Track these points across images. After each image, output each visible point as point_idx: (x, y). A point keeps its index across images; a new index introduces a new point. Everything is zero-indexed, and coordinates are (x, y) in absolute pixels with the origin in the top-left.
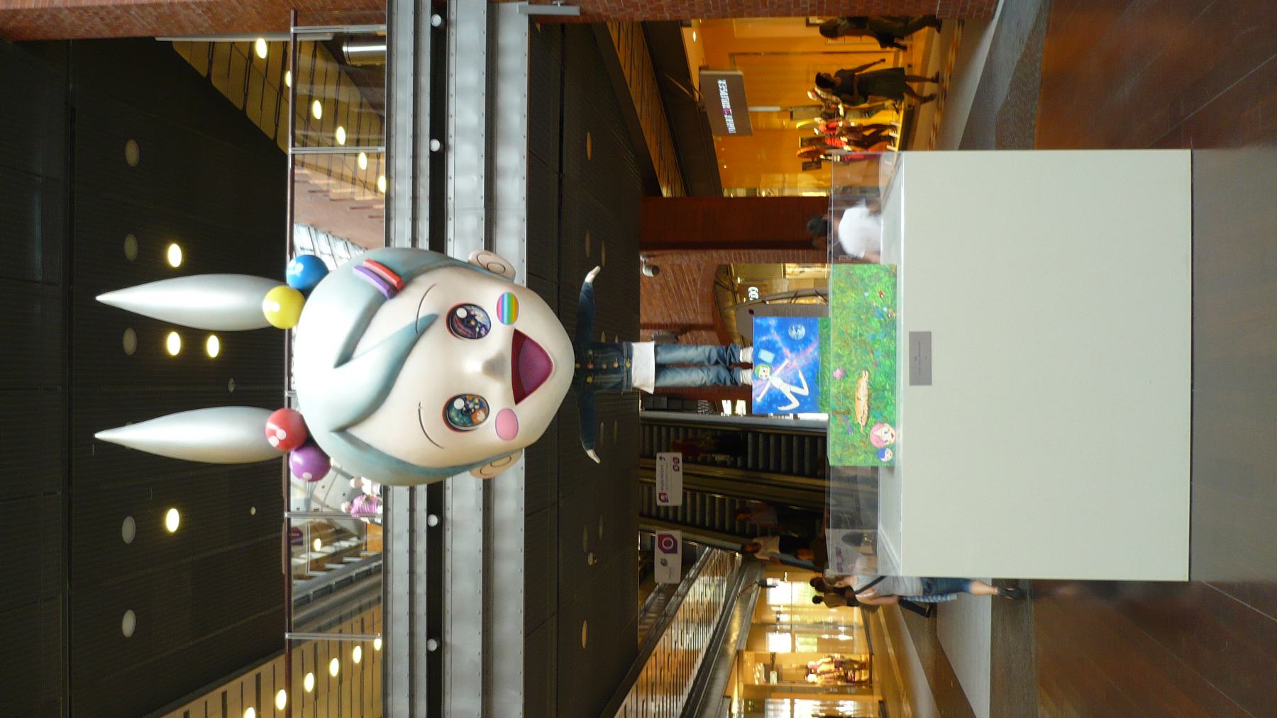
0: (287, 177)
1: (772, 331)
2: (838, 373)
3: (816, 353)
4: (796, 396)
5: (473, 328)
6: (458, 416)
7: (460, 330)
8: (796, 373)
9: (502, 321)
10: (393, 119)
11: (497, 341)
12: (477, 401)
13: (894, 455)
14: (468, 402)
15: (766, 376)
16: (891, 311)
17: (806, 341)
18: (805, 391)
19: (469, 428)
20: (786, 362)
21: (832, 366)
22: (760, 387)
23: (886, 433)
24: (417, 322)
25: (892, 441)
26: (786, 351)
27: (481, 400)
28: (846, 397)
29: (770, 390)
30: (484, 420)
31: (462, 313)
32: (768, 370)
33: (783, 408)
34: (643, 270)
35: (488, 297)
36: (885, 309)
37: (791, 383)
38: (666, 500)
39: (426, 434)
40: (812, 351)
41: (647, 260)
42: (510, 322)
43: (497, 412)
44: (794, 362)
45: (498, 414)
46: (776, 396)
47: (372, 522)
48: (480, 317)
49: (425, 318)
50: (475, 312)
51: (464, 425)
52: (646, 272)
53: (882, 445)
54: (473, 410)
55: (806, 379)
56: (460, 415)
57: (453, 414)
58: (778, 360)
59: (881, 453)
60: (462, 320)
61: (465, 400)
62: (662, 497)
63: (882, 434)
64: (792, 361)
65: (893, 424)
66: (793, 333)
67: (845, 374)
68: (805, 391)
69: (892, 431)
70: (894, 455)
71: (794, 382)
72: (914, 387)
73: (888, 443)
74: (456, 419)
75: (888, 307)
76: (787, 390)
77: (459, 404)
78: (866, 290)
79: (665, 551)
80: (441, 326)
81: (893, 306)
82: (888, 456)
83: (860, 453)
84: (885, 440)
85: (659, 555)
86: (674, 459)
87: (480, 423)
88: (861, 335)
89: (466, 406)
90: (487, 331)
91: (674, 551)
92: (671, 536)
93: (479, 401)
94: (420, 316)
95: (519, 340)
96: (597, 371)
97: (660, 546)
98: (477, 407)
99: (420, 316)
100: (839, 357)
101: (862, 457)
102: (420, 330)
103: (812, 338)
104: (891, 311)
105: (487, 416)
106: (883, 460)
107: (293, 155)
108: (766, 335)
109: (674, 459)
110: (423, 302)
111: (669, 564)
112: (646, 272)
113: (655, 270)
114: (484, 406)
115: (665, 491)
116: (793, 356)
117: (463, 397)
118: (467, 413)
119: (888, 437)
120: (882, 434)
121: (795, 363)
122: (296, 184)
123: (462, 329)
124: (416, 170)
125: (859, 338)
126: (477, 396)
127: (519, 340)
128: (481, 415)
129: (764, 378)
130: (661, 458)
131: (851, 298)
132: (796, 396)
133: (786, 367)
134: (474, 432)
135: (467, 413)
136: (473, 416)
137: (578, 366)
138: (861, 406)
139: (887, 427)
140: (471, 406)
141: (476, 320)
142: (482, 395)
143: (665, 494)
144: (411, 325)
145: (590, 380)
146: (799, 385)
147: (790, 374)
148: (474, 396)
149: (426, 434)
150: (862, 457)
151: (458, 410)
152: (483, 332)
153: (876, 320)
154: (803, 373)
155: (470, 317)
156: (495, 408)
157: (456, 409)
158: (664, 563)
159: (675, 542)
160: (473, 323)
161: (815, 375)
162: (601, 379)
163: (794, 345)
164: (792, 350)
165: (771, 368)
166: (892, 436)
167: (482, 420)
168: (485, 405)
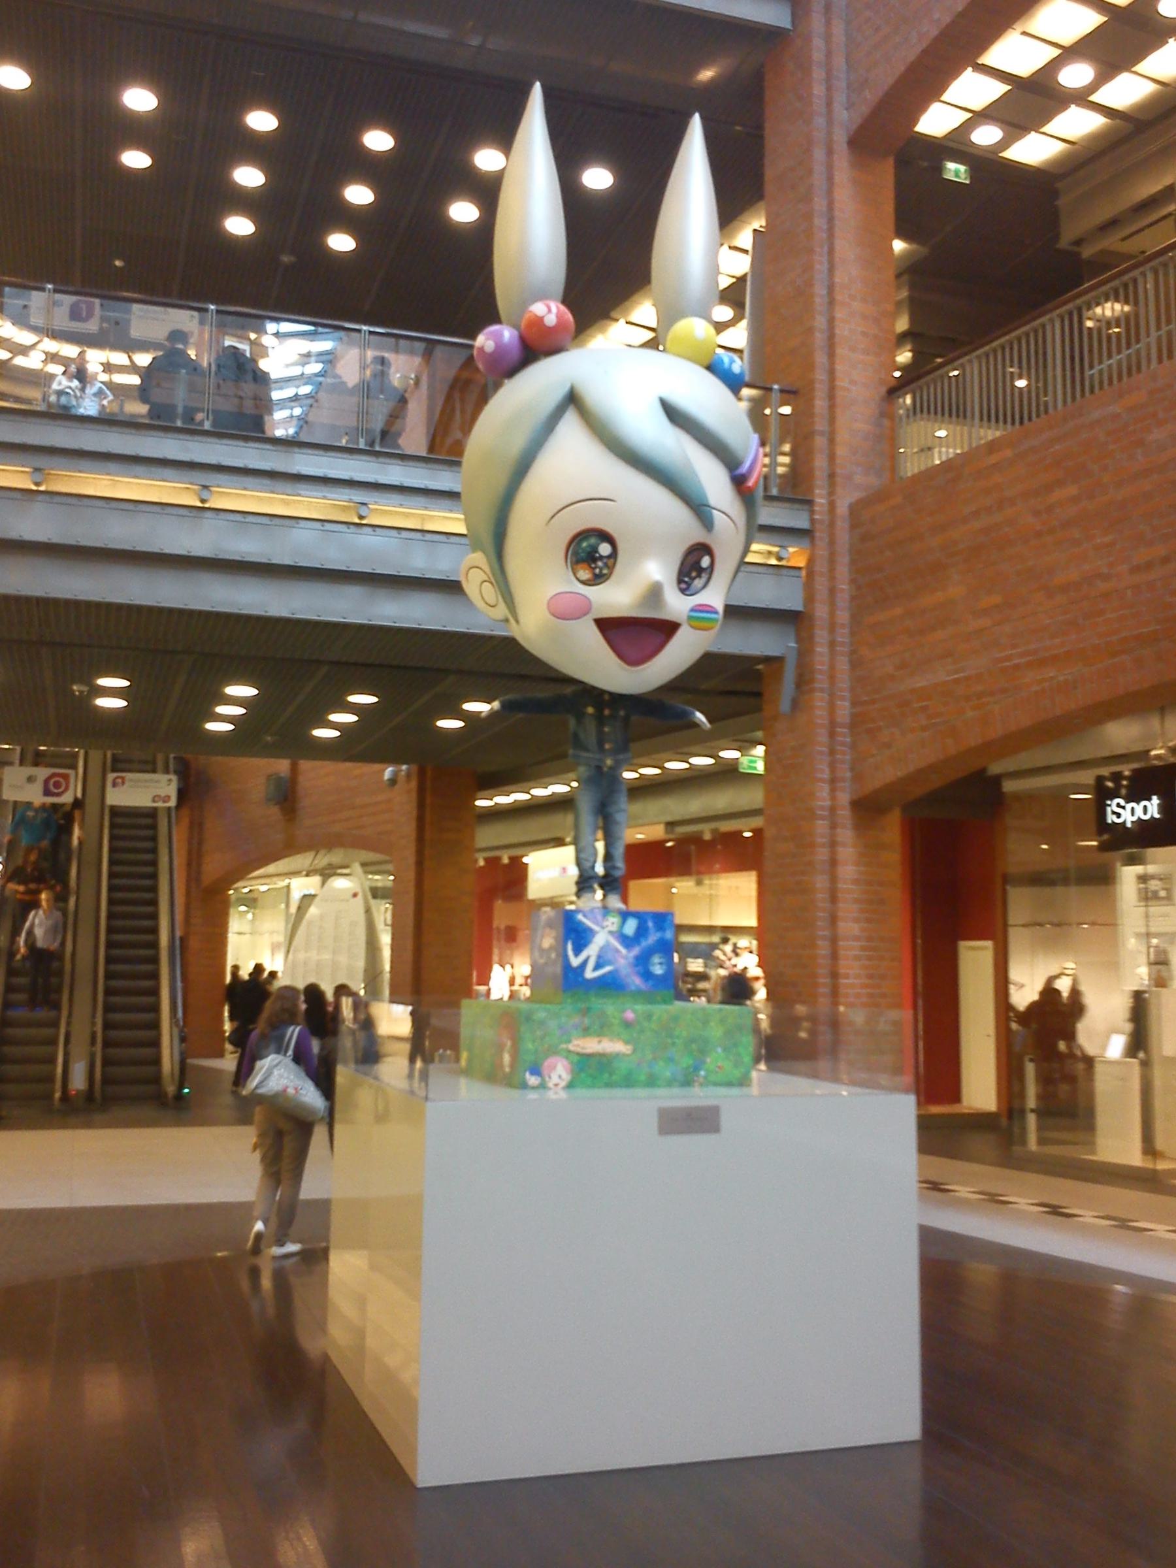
0: (335, 319)
1: (659, 935)
2: (630, 1015)
3: (633, 988)
4: (584, 964)
5: (688, 575)
6: (590, 546)
7: (690, 558)
8: (609, 963)
9: (692, 610)
10: (445, 467)
11: (677, 605)
12: (605, 571)
13: (533, 1088)
14: (605, 560)
15: (607, 926)
16: (701, 1080)
17: (647, 975)
18: (589, 974)
19: (569, 560)
20: (623, 951)
21: (639, 1007)
22: (595, 918)
23: (560, 1077)
24: (709, 506)
25: (551, 1085)
26: (636, 951)
27: (606, 577)
28: (602, 1027)
29: (591, 930)
30: (578, 579)
31: (705, 562)
32: (614, 928)
33: (570, 947)
34: (390, 769)
35: (714, 596)
36: (702, 1073)
37: (599, 957)
38: (114, 785)
39: (567, 506)
40: (636, 982)
41: (403, 773)
42: (690, 618)
43: (591, 598)
44: (624, 958)
45: (589, 599)
46: (583, 938)
47: (90, 398)
48: (698, 583)
49: (711, 514)
50: (704, 576)
51: (575, 553)
52: (388, 772)
53: (545, 1072)
54: (593, 566)
55: (604, 976)
56: (589, 549)
57: (593, 541)
58: (626, 941)
59: (536, 1071)
60: (698, 562)
61: (609, 557)
62: (119, 781)
63: (559, 1072)
64: (625, 958)
65: (570, 1086)
66: (656, 959)
67: (627, 1024)
68: (589, 974)
69: (563, 1084)
70: (533, 1088)
71: (601, 961)
72: (655, 1114)
73: (547, 1079)
74: (584, 544)
75: (705, 1077)
76: (591, 951)
77: (605, 549)
78: (724, 1050)
79: (46, 782)
80: (697, 535)
81: (706, 1083)
82: (533, 1080)
83: (536, 1044)
84: (552, 1075)
85: (42, 773)
86: (169, 797)
87: (575, 574)
88: (674, 1044)
89: (601, 558)
90: (683, 591)
91: (47, 792)
92: (66, 789)
93: (605, 575)
94: (715, 512)
95: (668, 628)
96: (600, 720)
97: (54, 775)
98: (597, 571)
99: (715, 512)
100: (649, 1017)
101: (530, 1046)
102: (700, 509)
103: (651, 983)
104: (701, 1080)
105: (584, 583)
106: (527, 1075)
107: (359, 331)
108: (655, 926)
109: (169, 797)
110: (724, 516)
111: (29, 786)
112: (388, 772)
113: (393, 781)
114: (598, 579)
115: (127, 784)
116: (631, 960)
117: (614, 554)
118: (591, 558)
119: (555, 1079)
120: (559, 1072)
121: (622, 962)
122: (393, 340)
123: (691, 559)
124: (334, 483)
125: (669, 1041)
126: (611, 574)
127: (668, 628)
128: (585, 574)
129: (605, 923)
130: (170, 780)
131: (716, 1032)
132: (584, 964)
133: (617, 951)
134: (564, 564)
135: (591, 558)
136: (585, 565)
137: (606, 697)
138: (591, 1045)
139: (566, 1077)
140: (600, 564)
141: (694, 578)
142: (613, 578)
143: (123, 783)
144: (707, 500)
145: (590, 710)
146: (598, 967)
147: (610, 956)
148: (612, 568)
149: (567, 506)
150: (530, 1046)
151: (597, 548)
152: (683, 586)
153: (691, 1062)
154: (610, 973)
155: (700, 571)
156: (592, 592)
157: (598, 545)
158: (31, 779)
159: (58, 795)
160: (694, 574)
161: (610, 985)
162: (591, 726)
163: (642, 961)
164: (637, 958)
165: (617, 932)
166: (556, 1085)
167: (578, 576)
168: (599, 581)
